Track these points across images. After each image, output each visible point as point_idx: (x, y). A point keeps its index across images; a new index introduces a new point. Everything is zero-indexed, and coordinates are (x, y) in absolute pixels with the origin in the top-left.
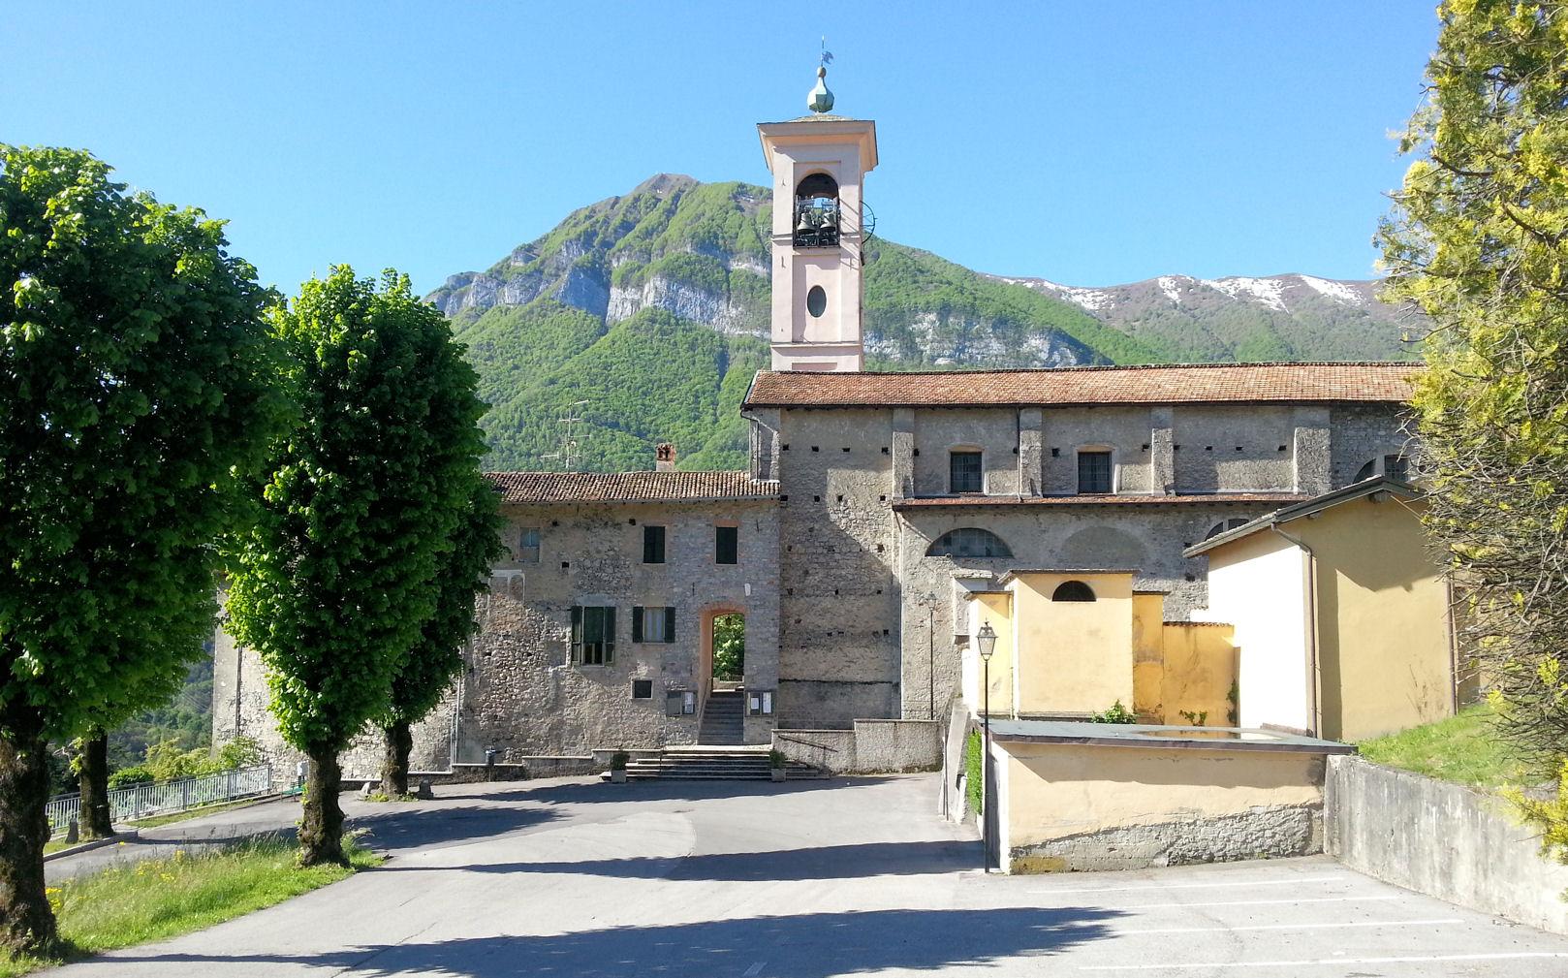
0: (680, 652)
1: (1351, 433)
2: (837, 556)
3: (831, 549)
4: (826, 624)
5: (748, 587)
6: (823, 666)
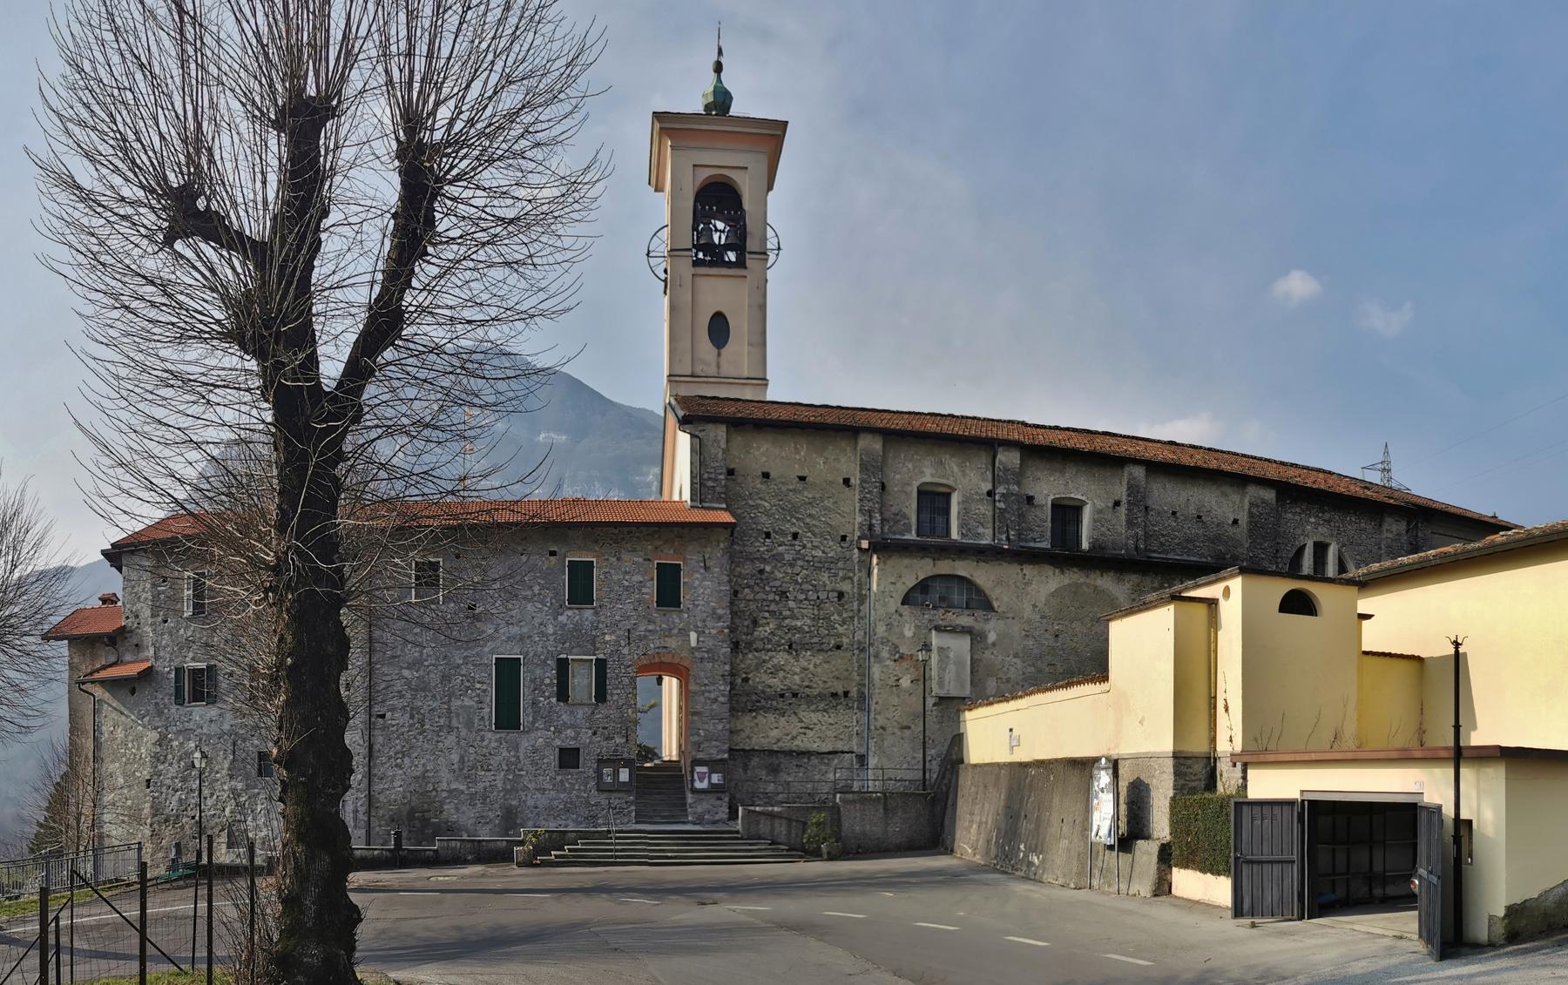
2: (791, 604)
3: (783, 594)
4: (776, 683)
5: (693, 636)
6: (774, 733)
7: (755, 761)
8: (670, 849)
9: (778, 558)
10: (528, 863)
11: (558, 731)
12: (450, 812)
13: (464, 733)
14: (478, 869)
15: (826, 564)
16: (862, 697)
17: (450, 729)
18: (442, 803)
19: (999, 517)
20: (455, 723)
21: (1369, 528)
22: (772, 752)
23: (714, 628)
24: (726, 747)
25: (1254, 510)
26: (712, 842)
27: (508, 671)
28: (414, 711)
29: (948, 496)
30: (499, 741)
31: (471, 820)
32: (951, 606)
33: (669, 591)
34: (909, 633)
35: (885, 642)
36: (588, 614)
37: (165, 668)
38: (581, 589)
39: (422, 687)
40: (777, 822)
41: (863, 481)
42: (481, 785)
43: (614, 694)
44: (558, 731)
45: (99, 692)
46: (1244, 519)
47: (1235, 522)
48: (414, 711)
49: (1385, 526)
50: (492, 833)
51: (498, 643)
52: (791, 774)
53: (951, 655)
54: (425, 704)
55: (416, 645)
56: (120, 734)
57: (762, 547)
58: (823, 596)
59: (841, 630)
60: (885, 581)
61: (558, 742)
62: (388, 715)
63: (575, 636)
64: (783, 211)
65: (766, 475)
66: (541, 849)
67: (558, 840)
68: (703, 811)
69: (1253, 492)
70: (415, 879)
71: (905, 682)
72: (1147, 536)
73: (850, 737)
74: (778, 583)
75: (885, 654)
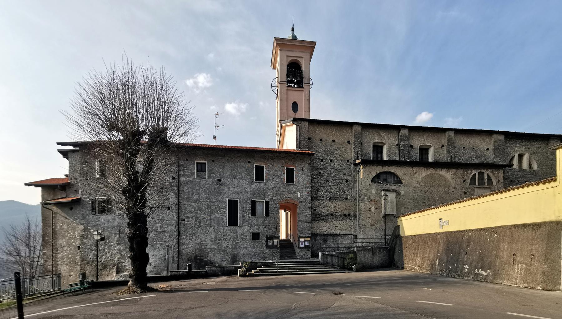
0: (272, 221)
1: (508, 145)
2: (330, 184)
3: (327, 181)
4: (325, 211)
5: (299, 194)
6: (325, 228)
7: (319, 238)
8: (297, 269)
9: (325, 168)
10: (244, 275)
11: (252, 227)
12: (211, 257)
13: (216, 227)
14: (224, 278)
15: (342, 170)
16: (355, 216)
17: (211, 225)
18: (208, 253)
19: (401, 152)
20: (213, 223)
21: (542, 146)
22: (324, 235)
23: (306, 191)
24: (310, 232)
25: (496, 144)
26: (309, 265)
27: (233, 205)
28: (197, 219)
29: (382, 148)
30: (230, 230)
31: (220, 259)
32: (387, 183)
33: (290, 178)
34: (374, 192)
35: (366, 195)
36: (262, 185)
37: (86, 198)
38: (260, 175)
39: (200, 210)
40: (334, 258)
41: (355, 141)
42: (223, 246)
43: (272, 213)
44: (252, 227)
45: (55, 209)
46: (491, 148)
47: (488, 149)
48: (197, 219)
49: (551, 144)
50: (227, 264)
51: (229, 194)
52: (332, 243)
53: (389, 199)
54: (201, 216)
55: (197, 193)
56: (65, 227)
57: (320, 164)
58: (341, 181)
59: (347, 193)
60: (364, 175)
61: (252, 231)
62: (186, 220)
63: (258, 193)
64: (315, 69)
65: (321, 140)
66: (249, 270)
67: (254, 266)
68: (302, 255)
69: (495, 137)
70: (197, 284)
71: (373, 209)
72: (455, 157)
73: (351, 230)
74: (325, 177)
75: (365, 199)
